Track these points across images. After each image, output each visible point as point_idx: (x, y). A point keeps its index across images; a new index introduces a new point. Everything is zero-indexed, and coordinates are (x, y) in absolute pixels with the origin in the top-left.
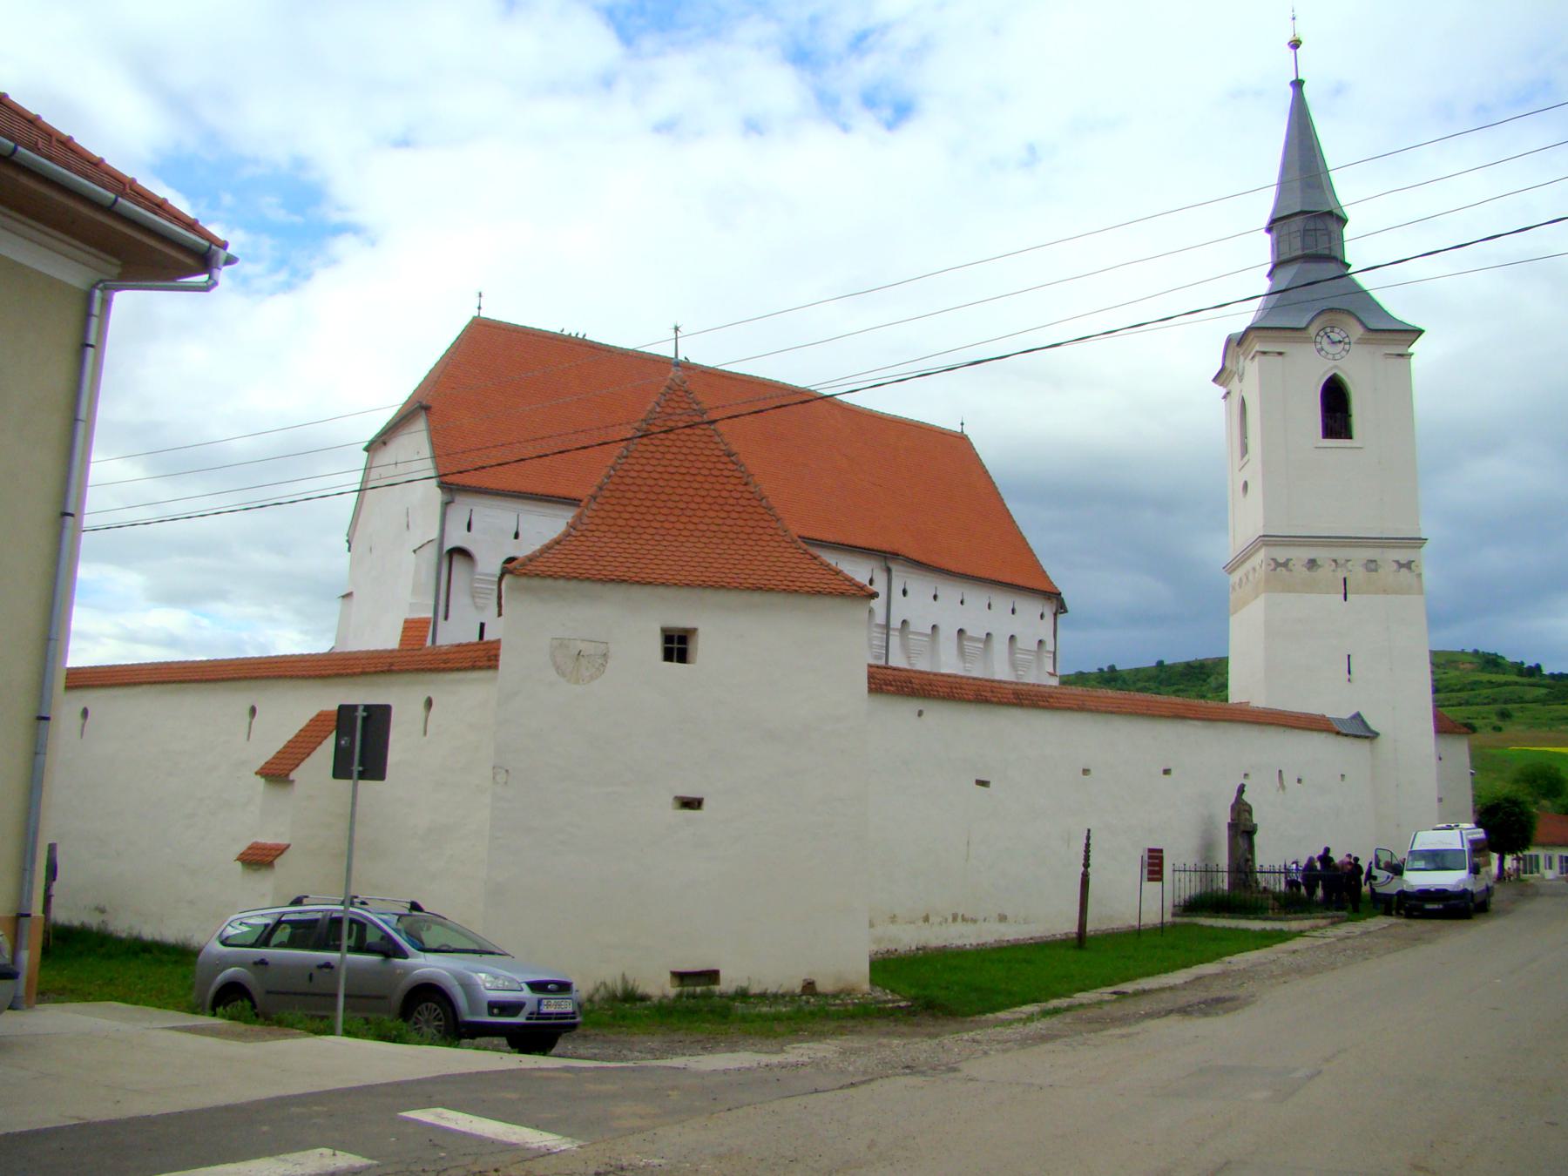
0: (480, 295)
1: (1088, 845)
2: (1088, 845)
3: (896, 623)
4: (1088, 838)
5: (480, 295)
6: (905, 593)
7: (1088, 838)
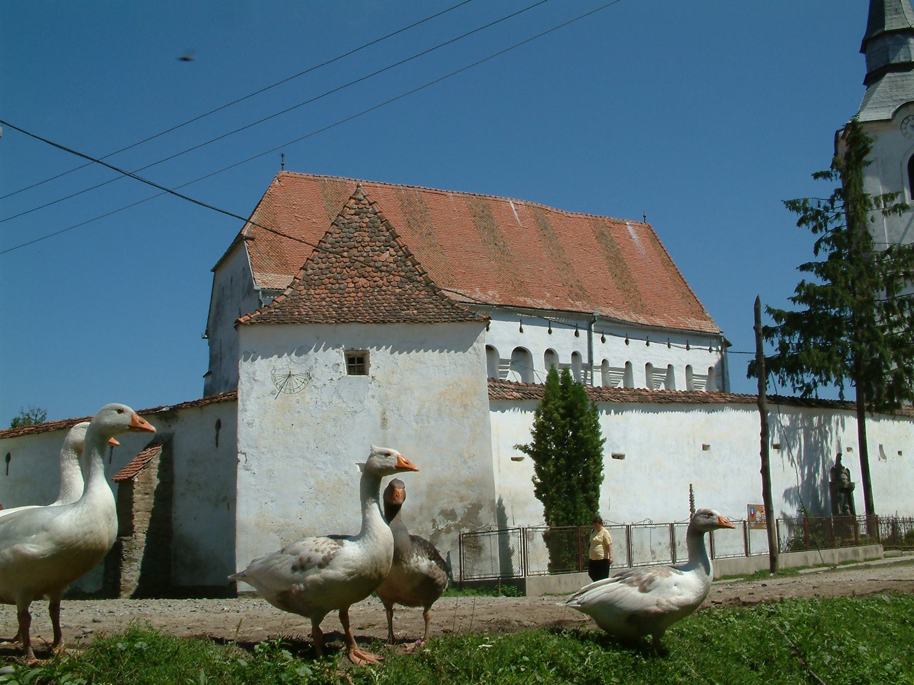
0: (283, 155)
1: (691, 496)
2: (691, 496)
3: (597, 362)
4: (691, 491)
5: (283, 155)
6: (603, 340)
7: (691, 491)
